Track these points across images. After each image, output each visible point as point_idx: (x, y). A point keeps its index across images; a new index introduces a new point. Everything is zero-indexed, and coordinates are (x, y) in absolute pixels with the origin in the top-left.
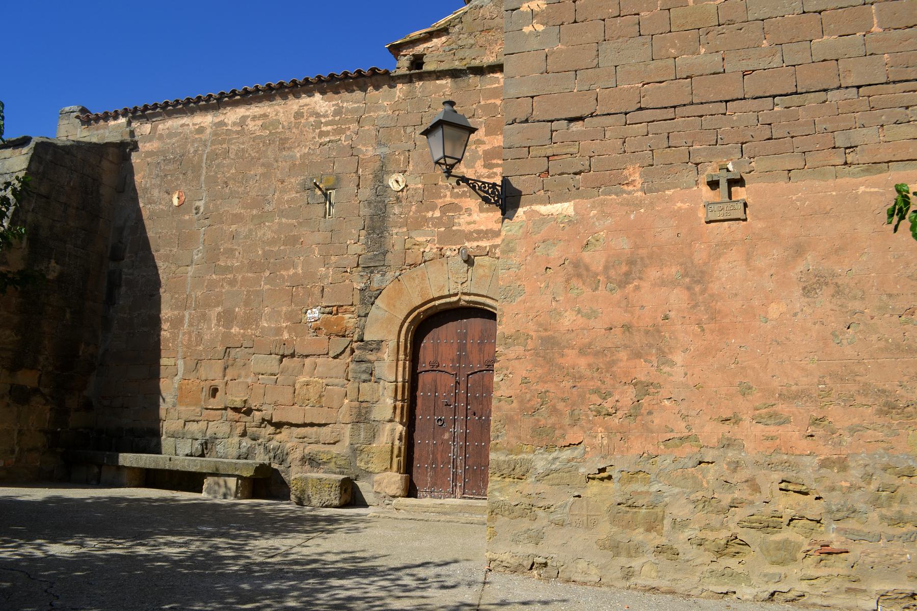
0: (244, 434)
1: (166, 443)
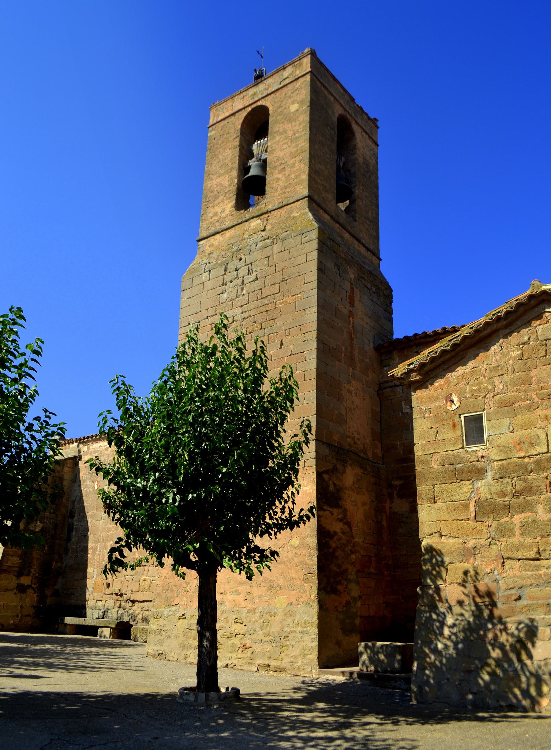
0: (120, 607)
1: (89, 612)
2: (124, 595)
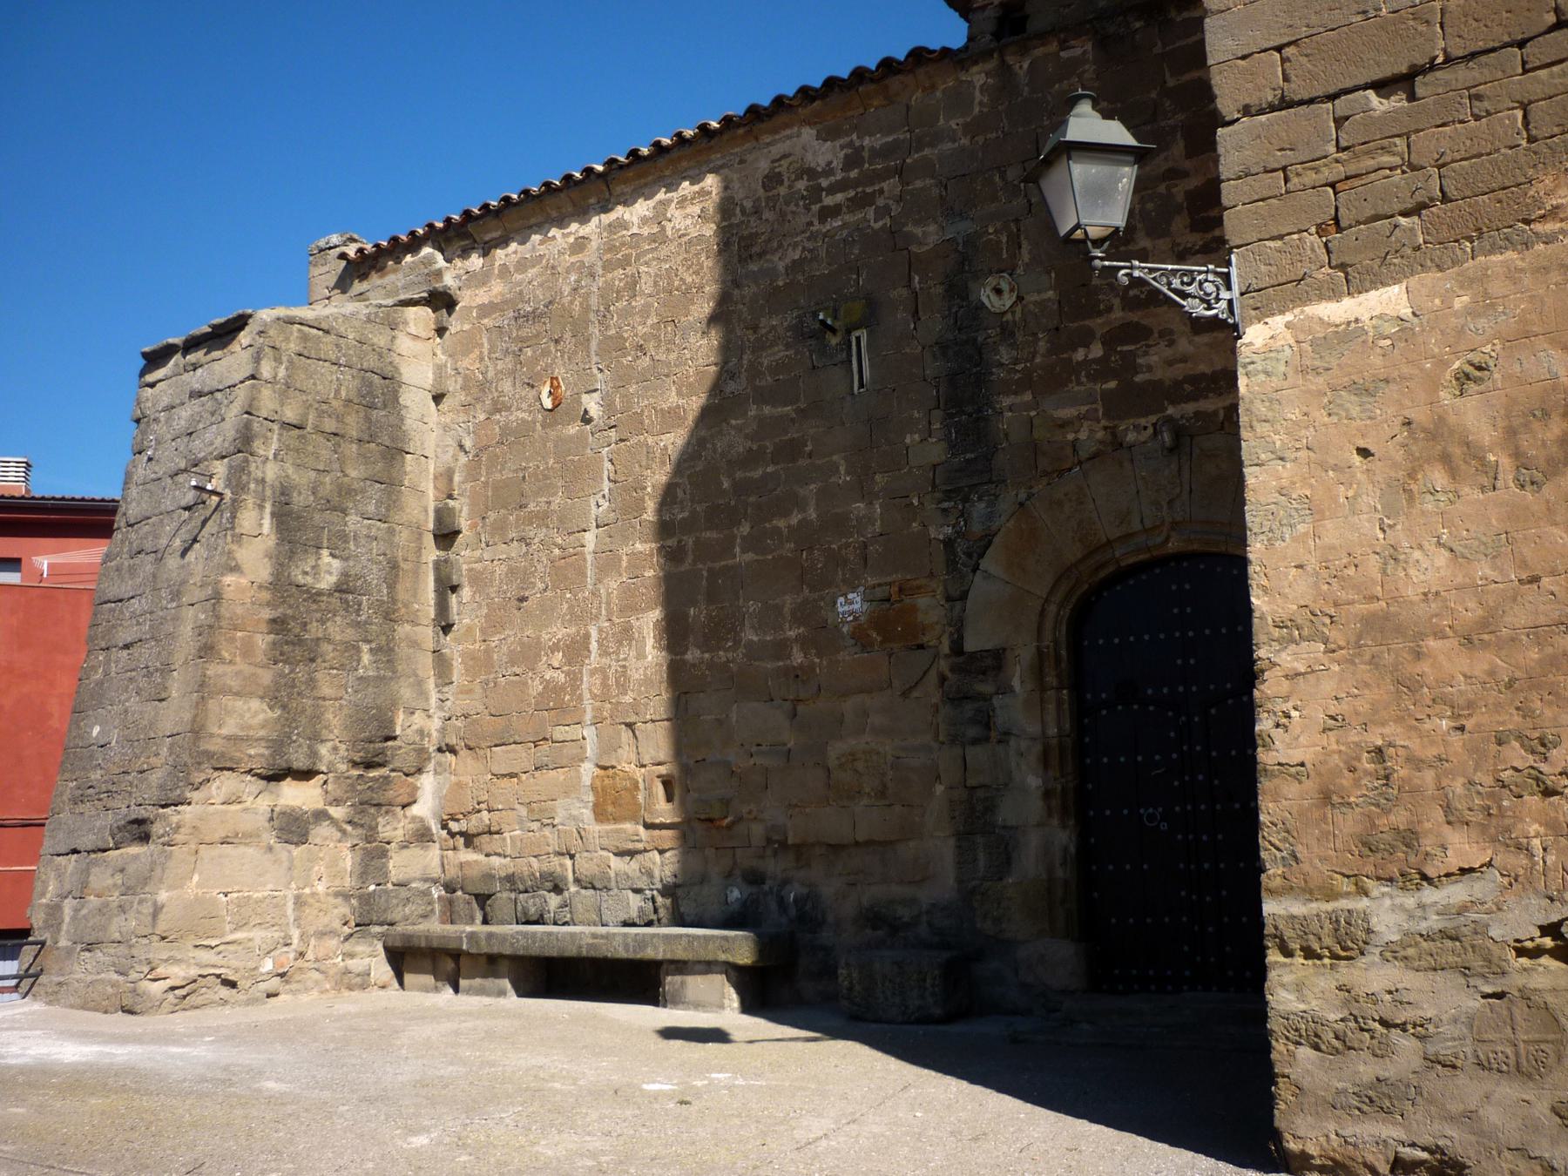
2: (1036, 435)
